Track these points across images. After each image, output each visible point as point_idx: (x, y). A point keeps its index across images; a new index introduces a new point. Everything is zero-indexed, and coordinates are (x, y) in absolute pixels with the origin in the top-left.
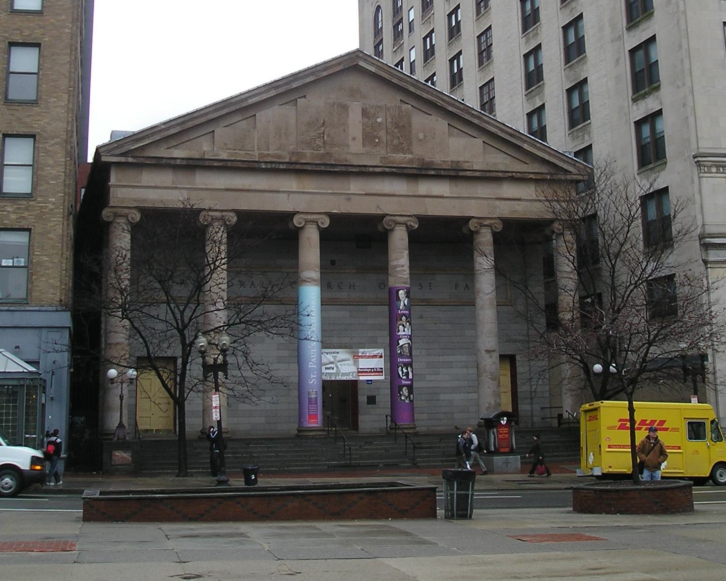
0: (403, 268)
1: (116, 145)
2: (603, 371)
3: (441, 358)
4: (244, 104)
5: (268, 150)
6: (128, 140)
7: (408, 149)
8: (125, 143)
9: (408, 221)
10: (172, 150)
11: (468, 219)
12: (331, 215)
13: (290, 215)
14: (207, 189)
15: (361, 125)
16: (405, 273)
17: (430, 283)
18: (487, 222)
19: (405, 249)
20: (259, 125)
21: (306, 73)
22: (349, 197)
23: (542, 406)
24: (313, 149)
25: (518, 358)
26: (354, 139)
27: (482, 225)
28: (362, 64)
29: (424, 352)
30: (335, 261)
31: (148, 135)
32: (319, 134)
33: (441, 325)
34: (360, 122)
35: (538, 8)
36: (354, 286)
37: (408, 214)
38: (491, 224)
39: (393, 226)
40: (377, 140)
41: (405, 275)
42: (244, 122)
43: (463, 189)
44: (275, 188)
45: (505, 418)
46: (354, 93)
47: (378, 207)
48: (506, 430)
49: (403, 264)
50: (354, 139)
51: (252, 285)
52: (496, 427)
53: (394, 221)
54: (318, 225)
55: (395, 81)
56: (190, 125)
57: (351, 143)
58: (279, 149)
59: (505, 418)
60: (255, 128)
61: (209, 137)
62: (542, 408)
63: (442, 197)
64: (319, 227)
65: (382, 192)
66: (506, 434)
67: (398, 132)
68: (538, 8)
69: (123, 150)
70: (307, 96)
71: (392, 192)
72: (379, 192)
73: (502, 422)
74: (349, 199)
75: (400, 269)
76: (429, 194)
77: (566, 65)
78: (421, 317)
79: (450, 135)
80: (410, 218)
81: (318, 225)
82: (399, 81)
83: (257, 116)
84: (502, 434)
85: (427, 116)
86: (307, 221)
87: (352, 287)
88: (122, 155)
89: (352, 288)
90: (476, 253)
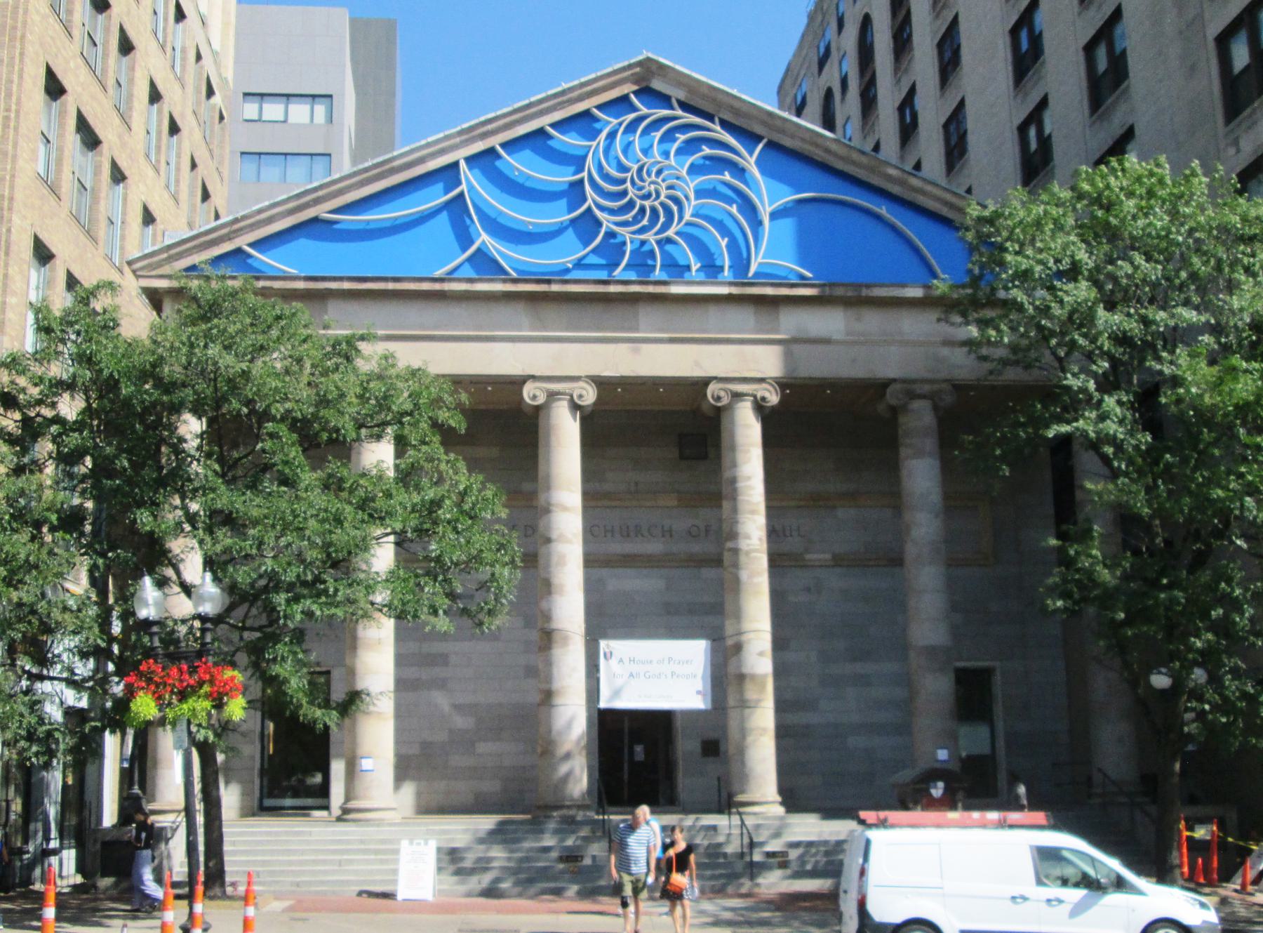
13: (517, 383)
18: (927, 388)
27: (913, 396)
43: (873, 321)
45: (941, 785)
59: (941, 785)
63: (826, 341)
86: (552, 395)
90: (903, 452)
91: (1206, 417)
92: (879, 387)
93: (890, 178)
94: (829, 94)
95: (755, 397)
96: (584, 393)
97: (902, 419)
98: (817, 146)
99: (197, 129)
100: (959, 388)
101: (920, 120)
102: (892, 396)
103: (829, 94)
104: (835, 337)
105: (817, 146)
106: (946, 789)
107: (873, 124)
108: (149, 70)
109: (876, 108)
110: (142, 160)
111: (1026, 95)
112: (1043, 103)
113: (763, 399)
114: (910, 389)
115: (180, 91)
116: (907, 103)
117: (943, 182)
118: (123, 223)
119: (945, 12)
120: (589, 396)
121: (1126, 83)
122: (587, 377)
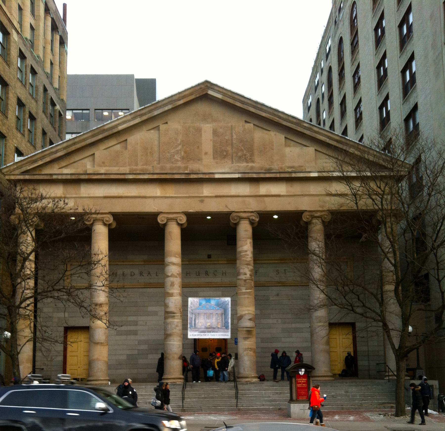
0: (246, 253)
1: (16, 166)
2: (413, 329)
3: (294, 325)
4: (115, 130)
5: (137, 166)
6: (25, 162)
7: (251, 159)
8: (23, 165)
9: (250, 216)
10: (63, 169)
11: (302, 212)
12: (187, 214)
13: (155, 215)
14: (90, 197)
15: (212, 142)
16: (248, 256)
17: (285, 270)
18: (318, 214)
19: (248, 238)
20: (129, 147)
21: (165, 102)
22: (202, 199)
23: (378, 362)
24: (172, 163)
25: (358, 325)
26: (206, 153)
27: (313, 217)
28: (210, 92)
29: (280, 321)
30: (210, 255)
31: (40, 158)
32: (178, 150)
33: (294, 301)
34: (211, 140)
35: (418, 123)
36: (225, 273)
37: (251, 210)
38: (321, 215)
39: (238, 221)
40: (225, 154)
41: (247, 258)
42: (119, 145)
43: (297, 188)
44: (143, 194)
45: (303, 370)
46: (205, 118)
47: (226, 206)
48: (304, 380)
49: (246, 250)
50: (206, 153)
51: (149, 274)
52: (294, 377)
53: (239, 217)
54: (177, 222)
55: (238, 104)
56: (73, 148)
57: (204, 157)
58: (146, 164)
59: (303, 370)
60: (126, 148)
61: (91, 158)
62: (377, 364)
63: (279, 196)
64: (179, 224)
65: (229, 194)
66: (304, 383)
67: (242, 145)
68: (418, 123)
69: (24, 169)
70: (168, 123)
71: (237, 194)
72: (226, 194)
73: (300, 373)
74: (202, 201)
75: (244, 254)
76: (268, 194)
77: (404, 100)
78: (278, 295)
79: (286, 145)
80: (252, 214)
81: (177, 222)
82: (242, 104)
83: (128, 141)
84: (300, 383)
85: (267, 132)
86: (169, 220)
87: (224, 274)
88: (24, 173)
89: (224, 274)
90: (310, 239)
91: (311, 317)
92: (298, 214)
93: (305, 128)
94: (318, 100)
95: (249, 219)
96: (181, 218)
97: (310, 227)
98: (275, 115)
99: (45, 119)
100: (332, 212)
101: (421, 127)
102: (305, 218)
103: (318, 100)
104: (282, 194)
105: (275, 115)
106: (305, 371)
107: (332, 112)
108: (16, 94)
109: (333, 105)
110: (15, 130)
111: (382, 94)
112: (415, 108)
113: (253, 220)
114: (312, 214)
115: (35, 103)
116: (343, 103)
117: (329, 130)
118: (5, 155)
119: (355, 62)
120: (183, 219)
121: (415, 84)
122: (182, 212)
